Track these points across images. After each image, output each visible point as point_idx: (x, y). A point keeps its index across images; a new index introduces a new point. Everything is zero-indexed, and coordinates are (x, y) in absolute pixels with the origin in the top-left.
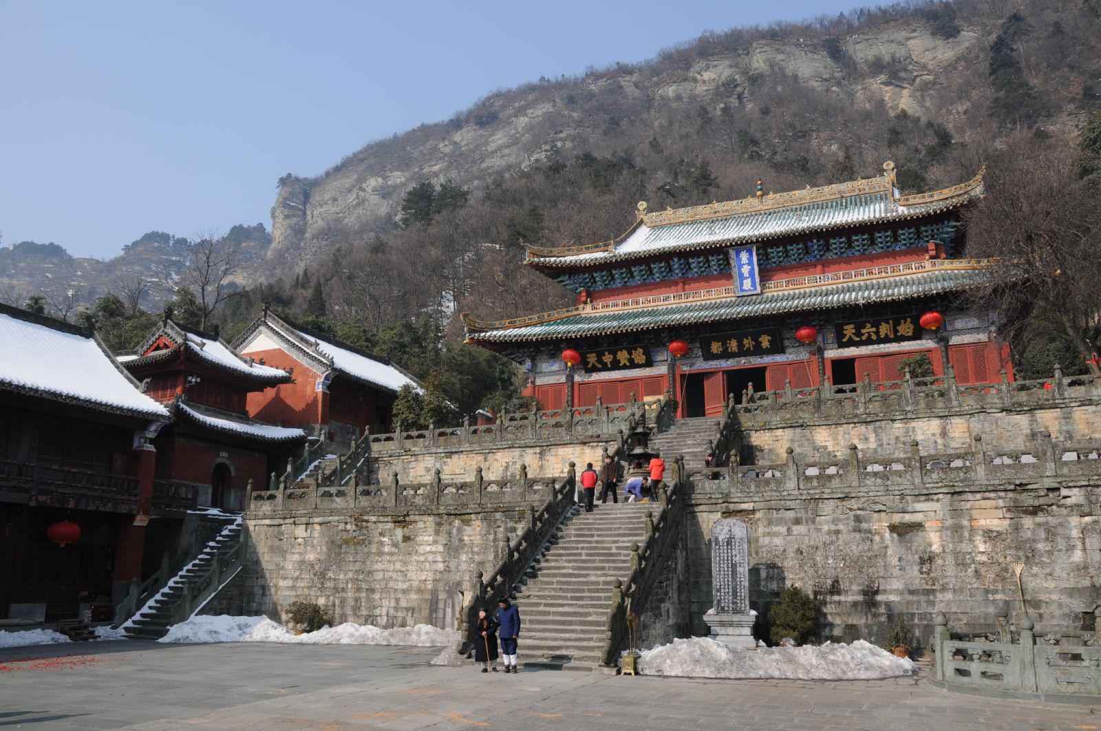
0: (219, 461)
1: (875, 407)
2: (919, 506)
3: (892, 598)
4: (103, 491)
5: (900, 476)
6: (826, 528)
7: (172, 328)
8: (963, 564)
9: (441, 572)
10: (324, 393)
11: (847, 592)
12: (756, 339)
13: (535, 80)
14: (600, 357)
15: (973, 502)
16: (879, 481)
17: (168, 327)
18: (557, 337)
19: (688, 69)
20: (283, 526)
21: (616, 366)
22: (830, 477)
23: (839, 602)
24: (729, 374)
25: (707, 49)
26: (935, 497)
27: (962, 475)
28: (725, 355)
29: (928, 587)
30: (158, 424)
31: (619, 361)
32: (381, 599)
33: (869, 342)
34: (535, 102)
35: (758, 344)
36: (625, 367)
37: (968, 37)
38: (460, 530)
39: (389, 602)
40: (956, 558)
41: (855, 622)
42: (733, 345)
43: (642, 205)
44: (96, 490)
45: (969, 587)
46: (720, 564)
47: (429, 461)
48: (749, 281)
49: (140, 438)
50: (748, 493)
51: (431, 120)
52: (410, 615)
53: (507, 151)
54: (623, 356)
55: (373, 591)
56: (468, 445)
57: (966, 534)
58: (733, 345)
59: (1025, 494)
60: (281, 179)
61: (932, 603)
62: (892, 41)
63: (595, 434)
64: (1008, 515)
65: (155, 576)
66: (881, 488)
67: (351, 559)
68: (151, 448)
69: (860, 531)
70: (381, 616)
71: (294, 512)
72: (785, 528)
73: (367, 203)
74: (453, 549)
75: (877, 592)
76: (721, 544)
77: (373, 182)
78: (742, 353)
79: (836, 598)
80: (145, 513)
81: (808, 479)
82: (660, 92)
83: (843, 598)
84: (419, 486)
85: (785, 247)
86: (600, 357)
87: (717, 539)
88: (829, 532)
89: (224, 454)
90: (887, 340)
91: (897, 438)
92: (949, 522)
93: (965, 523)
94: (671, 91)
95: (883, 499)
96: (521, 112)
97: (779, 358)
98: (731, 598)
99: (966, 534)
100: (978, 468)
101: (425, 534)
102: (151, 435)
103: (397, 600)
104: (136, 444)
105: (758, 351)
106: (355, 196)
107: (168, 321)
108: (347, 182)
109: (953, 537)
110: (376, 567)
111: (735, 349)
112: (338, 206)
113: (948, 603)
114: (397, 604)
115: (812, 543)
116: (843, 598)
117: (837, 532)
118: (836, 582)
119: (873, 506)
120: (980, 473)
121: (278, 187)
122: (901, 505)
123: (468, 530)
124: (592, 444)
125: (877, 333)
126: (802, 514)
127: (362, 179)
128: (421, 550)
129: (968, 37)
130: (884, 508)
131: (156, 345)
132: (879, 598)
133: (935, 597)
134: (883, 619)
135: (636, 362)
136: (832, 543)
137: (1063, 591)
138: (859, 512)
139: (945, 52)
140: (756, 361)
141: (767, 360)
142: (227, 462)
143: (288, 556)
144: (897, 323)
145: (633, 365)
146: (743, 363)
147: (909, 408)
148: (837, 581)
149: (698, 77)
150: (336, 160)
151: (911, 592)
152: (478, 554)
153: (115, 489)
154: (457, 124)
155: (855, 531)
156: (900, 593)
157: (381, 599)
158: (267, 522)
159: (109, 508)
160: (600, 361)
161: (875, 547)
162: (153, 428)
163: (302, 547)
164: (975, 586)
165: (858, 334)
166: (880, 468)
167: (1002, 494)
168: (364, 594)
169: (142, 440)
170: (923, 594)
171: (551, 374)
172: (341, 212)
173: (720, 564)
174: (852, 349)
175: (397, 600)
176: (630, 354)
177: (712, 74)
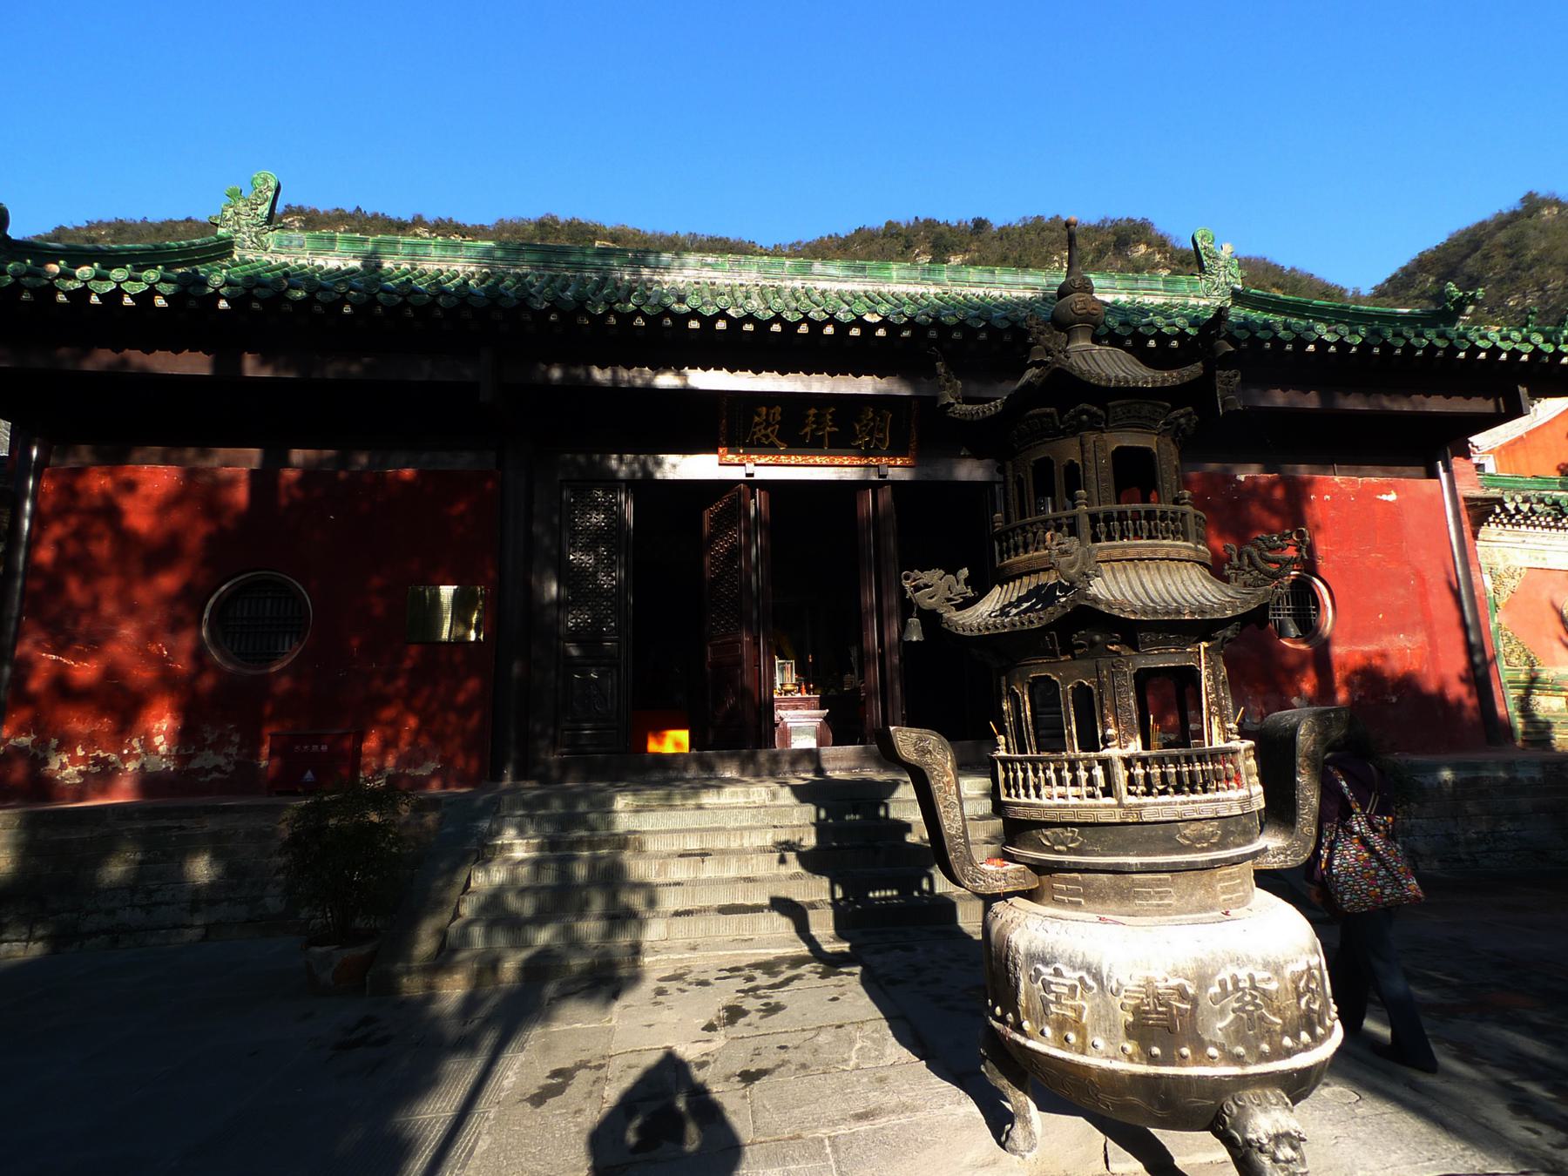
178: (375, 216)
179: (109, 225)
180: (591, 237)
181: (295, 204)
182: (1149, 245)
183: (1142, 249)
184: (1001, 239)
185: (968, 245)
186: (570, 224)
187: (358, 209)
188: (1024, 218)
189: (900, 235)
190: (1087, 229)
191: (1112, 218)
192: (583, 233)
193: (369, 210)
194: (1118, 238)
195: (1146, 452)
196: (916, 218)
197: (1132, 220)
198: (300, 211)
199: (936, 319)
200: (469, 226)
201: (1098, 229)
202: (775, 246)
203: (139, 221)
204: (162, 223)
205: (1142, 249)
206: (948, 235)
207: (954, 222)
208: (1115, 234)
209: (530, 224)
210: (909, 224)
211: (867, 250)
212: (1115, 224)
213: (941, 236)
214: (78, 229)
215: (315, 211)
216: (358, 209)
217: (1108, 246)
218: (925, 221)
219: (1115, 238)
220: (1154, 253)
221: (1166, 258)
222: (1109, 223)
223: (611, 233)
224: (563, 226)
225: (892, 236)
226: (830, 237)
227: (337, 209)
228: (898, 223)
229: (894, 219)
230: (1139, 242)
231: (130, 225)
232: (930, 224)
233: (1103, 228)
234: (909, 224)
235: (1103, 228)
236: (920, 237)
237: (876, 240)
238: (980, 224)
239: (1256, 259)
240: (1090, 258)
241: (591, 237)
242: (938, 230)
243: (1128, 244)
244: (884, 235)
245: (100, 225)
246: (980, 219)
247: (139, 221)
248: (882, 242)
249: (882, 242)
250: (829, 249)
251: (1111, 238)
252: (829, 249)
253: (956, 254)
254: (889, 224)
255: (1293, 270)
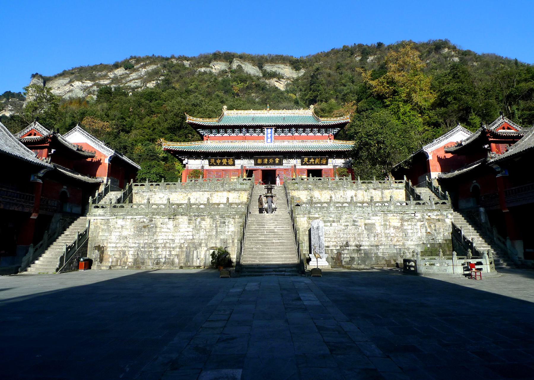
0: (63, 190)
1: (334, 185)
2: (373, 218)
3: (366, 248)
4: (18, 201)
5: (368, 208)
6: (343, 224)
7: (38, 125)
8: (387, 237)
9: (191, 239)
10: (109, 164)
11: (351, 246)
12: (274, 160)
13: (150, 55)
14: (216, 160)
15: (390, 216)
16: (361, 209)
17: (36, 125)
18: (208, 152)
19: (210, 63)
20: (110, 220)
21: (221, 164)
22: (345, 207)
23: (348, 249)
24: (264, 171)
25: (217, 57)
26: (379, 215)
27: (387, 208)
28: (262, 164)
29: (377, 244)
30: (46, 170)
31: (223, 163)
32: (162, 251)
33: (311, 164)
34: (151, 64)
35: (275, 161)
36: (224, 165)
37: (302, 72)
38: (200, 223)
39: (166, 252)
40: (385, 235)
41: (354, 256)
42: (266, 160)
43: (225, 107)
44: (14, 200)
45: (389, 244)
46: (314, 236)
47: (147, 195)
48: (270, 139)
49: (35, 176)
50: (317, 211)
51: (105, 62)
52: (176, 258)
53: (136, 81)
54: (225, 161)
55: (158, 248)
56: (180, 189)
57: (388, 227)
58: (266, 161)
59: (405, 215)
60: (33, 75)
61: (378, 249)
62: (280, 68)
63: (233, 188)
64: (400, 221)
65: (41, 243)
66: (362, 211)
67: (147, 234)
68: (40, 181)
69: (355, 225)
70: (162, 258)
71: (116, 214)
72: (330, 224)
73: (74, 92)
74: (197, 229)
75: (361, 246)
76: (315, 229)
77: (77, 84)
78: (268, 164)
79: (347, 248)
80: (37, 212)
81: (398, 206)
82: (199, 69)
83: (349, 248)
84: (181, 204)
85: (283, 129)
86: (216, 160)
87: (313, 227)
88: (345, 226)
89: (65, 187)
90: (317, 164)
91: (341, 196)
92: (383, 223)
93: (388, 223)
94: (203, 70)
95: (363, 215)
96: (144, 66)
97: (281, 167)
98: (318, 248)
99: (388, 227)
100: (391, 206)
101: (183, 224)
102: (40, 175)
103: (170, 251)
104: (32, 179)
105: (274, 164)
106: (68, 88)
107: (37, 122)
108: (67, 80)
109: (384, 228)
110: (159, 238)
111: (266, 162)
112: (59, 90)
113: (383, 249)
114: (170, 253)
115: (339, 229)
116: (349, 248)
117: (347, 225)
118: (347, 243)
119: (359, 217)
120: (392, 208)
121: (31, 78)
122: (368, 217)
123: (204, 222)
124: (232, 192)
125: (314, 162)
126: (335, 220)
127: (71, 82)
128: (181, 230)
129: (302, 72)
130: (363, 218)
131: (30, 133)
132: (362, 248)
133: (379, 247)
134: (363, 255)
135: (276, 160)
136: (345, 229)
137: (415, 245)
138: (355, 219)
139: (294, 75)
140: (273, 167)
141: (277, 167)
142: (67, 191)
143: (113, 234)
144: (321, 159)
145: (228, 164)
146: (269, 167)
147: (345, 187)
148: (347, 242)
149: (213, 67)
150: (60, 71)
151: (372, 246)
152: (208, 232)
153: (23, 200)
154: (116, 66)
155: (353, 225)
156: (369, 246)
157: (162, 251)
158: (102, 218)
159: (20, 209)
160: (215, 162)
161: (360, 231)
162: (42, 172)
163: (121, 229)
164: (391, 244)
165: (308, 161)
166: (361, 205)
167: (399, 215)
168: (153, 249)
169: (35, 177)
170: (375, 246)
171: (193, 164)
172: (61, 93)
173: (314, 236)
174: (306, 166)
175: (170, 251)
176: (227, 160)
177: (218, 67)
178: (159, 57)
179: (78, 68)
180: (232, 57)
181: (133, 55)
182: (449, 48)
183: (446, 50)
184: (389, 49)
185: (376, 52)
186: (225, 53)
187: (153, 55)
188: (397, 42)
189: (349, 50)
190: (423, 44)
191: (433, 39)
192: (229, 56)
193: (157, 55)
194: (436, 47)
195: (137, 169)
196: (355, 44)
197: (442, 40)
198: (135, 57)
199: (402, 43)
200: (190, 57)
201: (427, 44)
202: (301, 57)
203: (87, 66)
204: (93, 66)
205: (446, 50)
206: (367, 49)
207: (369, 45)
208: (434, 45)
209: (211, 55)
210: (352, 46)
211: (336, 56)
212: (434, 42)
213: (365, 49)
214: (69, 70)
215: (140, 57)
216: (153, 55)
217: (432, 49)
218: (358, 45)
219: (435, 47)
220: (451, 51)
221: (456, 53)
222: (432, 42)
223: (239, 55)
224: (222, 54)
225: (345, 51)
226: (322, 52)
227: (147, 56)
228: (348, 46)
229: (346, 45)
230: (445, 47)
231: (84, 68)
232: (360, 46)
233: (429, 43)
234: (352, 46)
235: (429, 43)
236: (356, 51)
237: (340, 53)
238: (380, 45)
239: (492, 54)
240: (425, 54)
241: (232, 57)
242: (363, 47)
243: (440, 48)
244: (343, 51)
245: (75, 68)
246: (380, 43)
247: (87, 66)
248: (342, 53)
249: (342, 53)
250: (321, 57)
251: (433, 47)
252: (321, 57)
253: (371, 56)
254: (344, 46)
255: (506, 58)
